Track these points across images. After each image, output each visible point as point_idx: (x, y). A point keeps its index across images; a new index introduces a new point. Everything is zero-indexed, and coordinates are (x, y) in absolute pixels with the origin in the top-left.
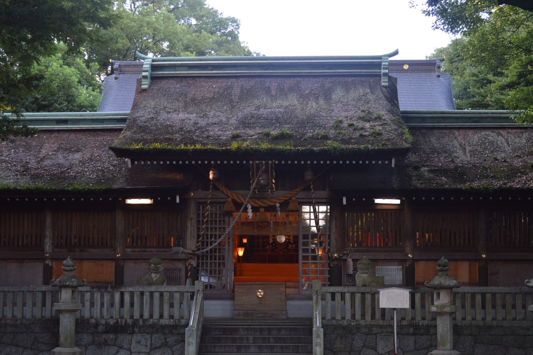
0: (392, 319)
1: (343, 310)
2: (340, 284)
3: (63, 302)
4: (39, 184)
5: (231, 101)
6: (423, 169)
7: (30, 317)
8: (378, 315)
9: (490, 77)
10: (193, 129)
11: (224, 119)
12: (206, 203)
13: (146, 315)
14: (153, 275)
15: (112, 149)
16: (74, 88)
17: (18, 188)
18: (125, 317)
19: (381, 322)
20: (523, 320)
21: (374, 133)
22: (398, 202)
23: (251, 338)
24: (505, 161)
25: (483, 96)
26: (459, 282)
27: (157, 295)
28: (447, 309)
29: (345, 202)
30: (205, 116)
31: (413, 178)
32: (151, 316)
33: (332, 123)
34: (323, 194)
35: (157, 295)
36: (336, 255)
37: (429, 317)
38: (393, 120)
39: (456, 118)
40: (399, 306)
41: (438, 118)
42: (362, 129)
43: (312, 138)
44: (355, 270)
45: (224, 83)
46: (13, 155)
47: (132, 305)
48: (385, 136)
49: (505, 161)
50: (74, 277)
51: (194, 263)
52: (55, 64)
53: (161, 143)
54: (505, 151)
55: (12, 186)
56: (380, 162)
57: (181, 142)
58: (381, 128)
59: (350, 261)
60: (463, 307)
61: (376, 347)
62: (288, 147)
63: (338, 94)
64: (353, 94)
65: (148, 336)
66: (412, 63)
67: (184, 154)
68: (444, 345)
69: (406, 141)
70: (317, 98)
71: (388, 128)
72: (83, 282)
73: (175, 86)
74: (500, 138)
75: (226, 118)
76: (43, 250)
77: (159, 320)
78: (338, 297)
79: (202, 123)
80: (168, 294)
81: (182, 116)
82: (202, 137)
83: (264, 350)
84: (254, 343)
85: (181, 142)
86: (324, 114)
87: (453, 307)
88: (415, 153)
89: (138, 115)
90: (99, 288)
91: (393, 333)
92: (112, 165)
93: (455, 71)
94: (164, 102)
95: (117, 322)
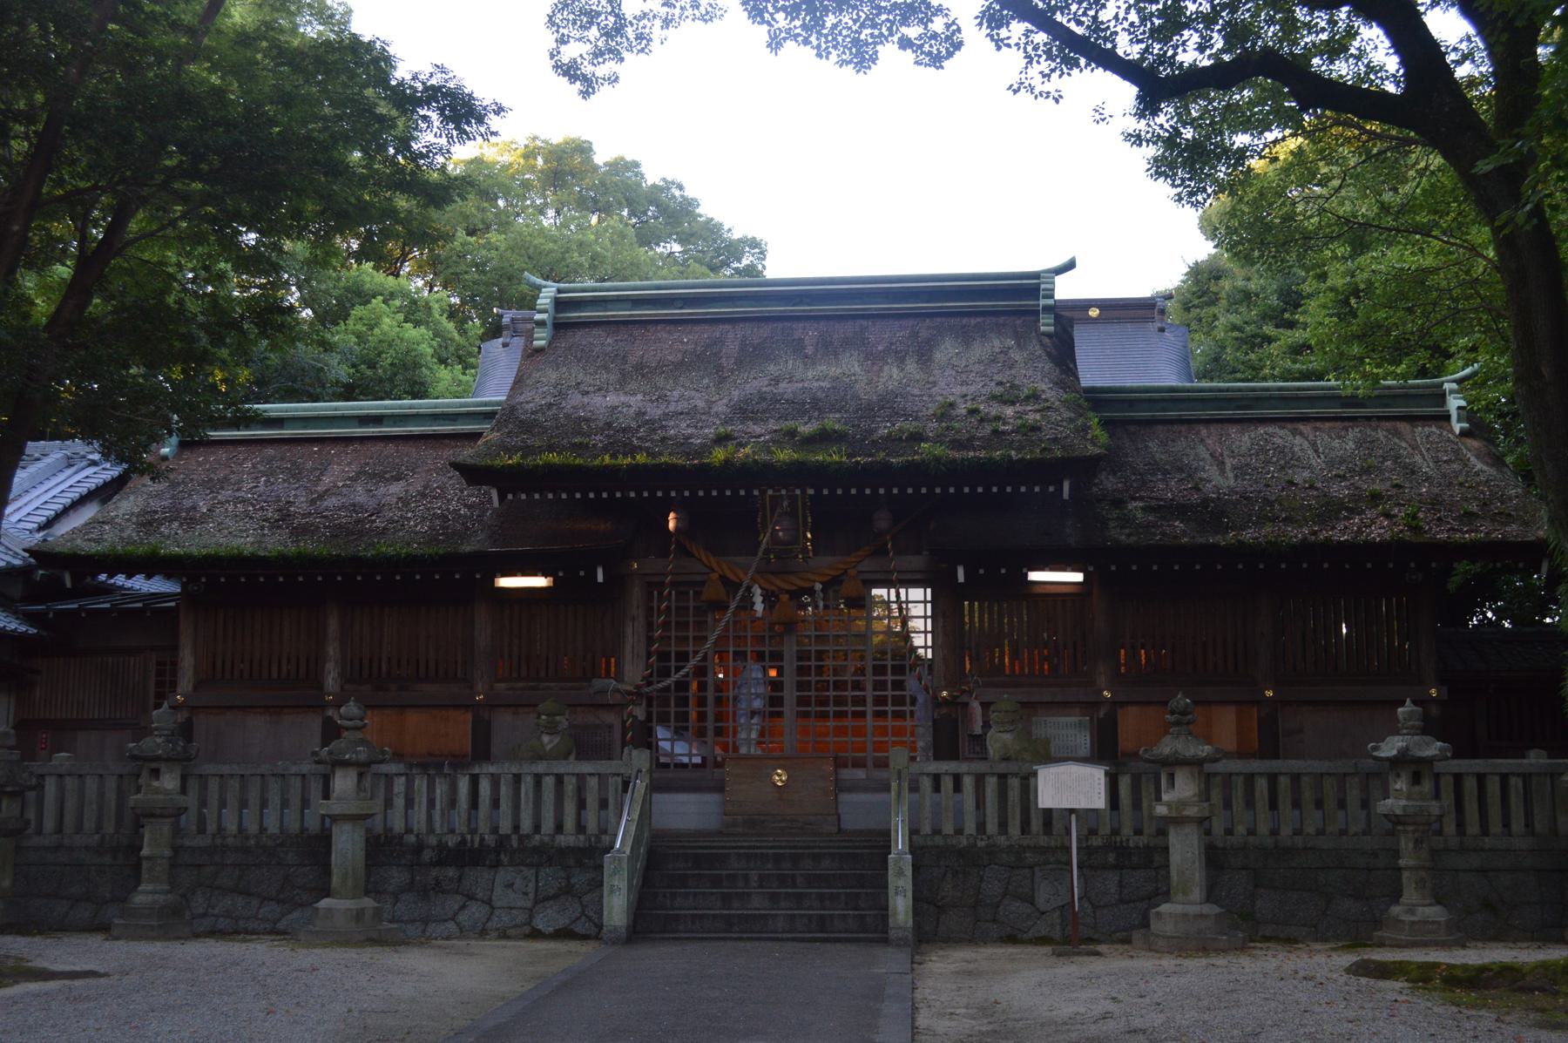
0: (1068, 832)
1: (959, 813)
2: (954, 756)
3: (339, 799)
4: (309, 546)
5: (719, 368)
6: (1132, 505)
7: (277, 831)
8: (1036, 824)
9: (1269, 329)
10: (634, 425)
11: (701, 404)
12: (662, 584)
13: (526, 825)
14: (546, 739)
15: (456, 466)
16: (429, 368)
17: (262, 554)
18: (481, 831)
19: (1043, 841)
20: (1364, 833)
21: (1023, 426)
22: (1078, 577)
23: (754, 875)
24: (1312, 487)
25: (1254, 369)
26: (1218, 751)
27: (549, 782)
28: (1192, 811)
29: (961, 578)
30: (663, 398)
31: (1112, 524)
32: (537, 828)
33: (932, 408)
34: (917, 562)
35: (549, 782)
36: (945, 694)
37: (1149, 829)
38: (1066, 401)
39: (1202, 400)
40: (1082, 804)
41: (1163, 400)
42: (998, 418)
43: (889, 438)
44: (987, 725)
45: (706, 333)
46: (262, 489)
47: (496, 803)
48: (1048, 434)
49: (1312, 487)
50: (362, 742)
51: (640, 713)
52: (387, 320)
53: (559, 453)
54: (1310, 467)
55: (248, 550)
56: (1037, 489)
57: (605, 449)
58: (1038, 417)
59: (976, 707)
60: (1228, 805)
61: (1033, 897)
62: (836, 458)
63: (947, 350)
64: (979, 351)
65: (530, 873)
66: (1108, 306)
67: (609, 475)
68: (1184, 893)
69: (1093, 441)
70: (901, 361)
71: (1054, 416)
72: (383, 752)
73: (604, 342)
74: (1298, 440)
75: (707, 401)
76: (319, 686)
77: (553, 837)
78: (947, 784)
79: (654, 412)
80: (574, 780)
81: (612, 399)
82: (652, 441)
83: (783, 904)
84: (761, 886)
85: (605, 449)
86: (916, 392)
87: (1206, 805)
88: (1114, 473)
89: (521, 399)
90: (424, 767)
91: (1070, 863)
92: (466, 506)
93: (1194, 326)
94: (577, 374)
95: (464, 841)
